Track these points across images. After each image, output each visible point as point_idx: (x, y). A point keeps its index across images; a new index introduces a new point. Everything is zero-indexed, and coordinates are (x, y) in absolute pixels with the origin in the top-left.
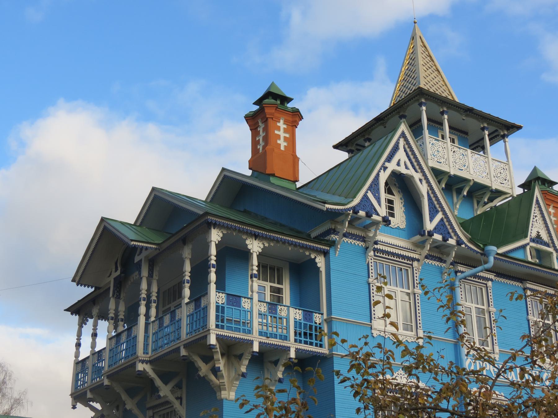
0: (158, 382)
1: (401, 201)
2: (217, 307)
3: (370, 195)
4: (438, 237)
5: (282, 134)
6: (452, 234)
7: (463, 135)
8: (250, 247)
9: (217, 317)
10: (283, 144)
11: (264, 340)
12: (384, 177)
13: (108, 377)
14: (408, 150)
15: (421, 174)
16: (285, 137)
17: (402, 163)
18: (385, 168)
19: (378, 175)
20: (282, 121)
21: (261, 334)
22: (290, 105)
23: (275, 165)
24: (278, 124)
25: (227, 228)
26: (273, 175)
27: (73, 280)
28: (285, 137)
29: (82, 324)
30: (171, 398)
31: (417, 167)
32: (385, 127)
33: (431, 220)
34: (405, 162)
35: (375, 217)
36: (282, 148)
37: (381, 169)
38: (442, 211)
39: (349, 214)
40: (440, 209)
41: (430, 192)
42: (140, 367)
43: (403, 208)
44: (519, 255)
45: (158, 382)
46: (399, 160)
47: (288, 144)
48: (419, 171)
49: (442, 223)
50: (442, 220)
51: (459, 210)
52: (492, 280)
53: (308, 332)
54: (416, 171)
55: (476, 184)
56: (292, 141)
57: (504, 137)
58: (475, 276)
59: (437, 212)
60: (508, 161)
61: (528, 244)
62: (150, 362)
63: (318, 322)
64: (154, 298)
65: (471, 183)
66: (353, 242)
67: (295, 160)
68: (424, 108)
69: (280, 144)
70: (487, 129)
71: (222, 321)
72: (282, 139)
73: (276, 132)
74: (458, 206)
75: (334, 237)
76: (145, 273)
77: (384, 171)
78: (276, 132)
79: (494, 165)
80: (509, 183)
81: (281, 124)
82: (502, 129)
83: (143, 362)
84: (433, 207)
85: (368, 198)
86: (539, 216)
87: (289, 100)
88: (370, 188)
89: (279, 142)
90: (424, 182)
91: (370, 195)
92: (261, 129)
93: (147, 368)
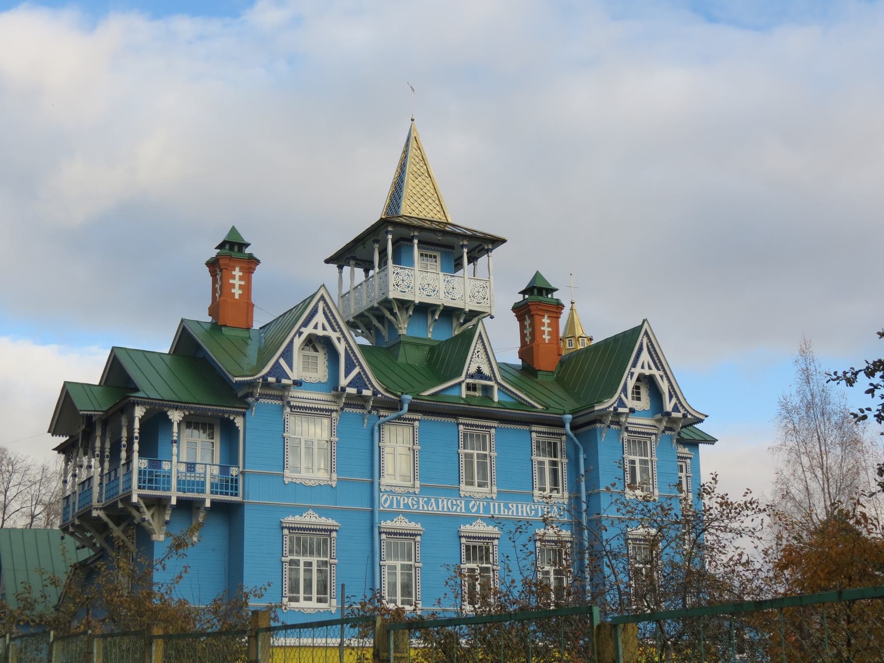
0: (111, 525)
2: (140, 472)
3: (282, 362)
4: (353, 391)
7: (451, 250)
8: (170, 417)
9: (139, 480)
10: (237, 292)
11: (181, 494)
12: (298, 342)
13: (78, 518)
16: (240, 285)
17: (320, 326)
18: (300, 334)
19: (292, 342)
20: (237, 269)
21: (179, 490)
22: (248, 251)
23: (229, 316)
24: (234, 273)
25: (148, 404)
26: (225, 326)
27: (49, 432)
28: (240, 285)
29: (340, 267)
30: (123, 537)
31: (336, 327)
33: (346, 377)
35: (284, 381)
36: (237, 297)
42: (95, 513)
44: (454, 393)
45: (111, 525)
50: (359, 373)
52: (418, 420)
53: (229, 484)
54: (334, 330)
55: (445, 307)
56: (247, 289)
57: (488, 251)
58: (399, 418)
59: (355, 366)
61: (463, 381)
62: (103, 509)
63: (234, 474)
64: (107, 453)
65: (441, 308)
66: (270, 401)
67: (250, 307)
68: (390, 237)
71: (144, 482)
73: (231, 281)
75: (250, 400)
76: (98, 433)
78: (231, 281)
81: (237, 273)
82: (482, 244)
83: (97, 509)
86: (482, 351)
87: (247, 245)
88: (281, 356)
89: (233, 291)
90: (342, 340)
91: (282, 362)
92: (218, 277)
93: (101, 514)
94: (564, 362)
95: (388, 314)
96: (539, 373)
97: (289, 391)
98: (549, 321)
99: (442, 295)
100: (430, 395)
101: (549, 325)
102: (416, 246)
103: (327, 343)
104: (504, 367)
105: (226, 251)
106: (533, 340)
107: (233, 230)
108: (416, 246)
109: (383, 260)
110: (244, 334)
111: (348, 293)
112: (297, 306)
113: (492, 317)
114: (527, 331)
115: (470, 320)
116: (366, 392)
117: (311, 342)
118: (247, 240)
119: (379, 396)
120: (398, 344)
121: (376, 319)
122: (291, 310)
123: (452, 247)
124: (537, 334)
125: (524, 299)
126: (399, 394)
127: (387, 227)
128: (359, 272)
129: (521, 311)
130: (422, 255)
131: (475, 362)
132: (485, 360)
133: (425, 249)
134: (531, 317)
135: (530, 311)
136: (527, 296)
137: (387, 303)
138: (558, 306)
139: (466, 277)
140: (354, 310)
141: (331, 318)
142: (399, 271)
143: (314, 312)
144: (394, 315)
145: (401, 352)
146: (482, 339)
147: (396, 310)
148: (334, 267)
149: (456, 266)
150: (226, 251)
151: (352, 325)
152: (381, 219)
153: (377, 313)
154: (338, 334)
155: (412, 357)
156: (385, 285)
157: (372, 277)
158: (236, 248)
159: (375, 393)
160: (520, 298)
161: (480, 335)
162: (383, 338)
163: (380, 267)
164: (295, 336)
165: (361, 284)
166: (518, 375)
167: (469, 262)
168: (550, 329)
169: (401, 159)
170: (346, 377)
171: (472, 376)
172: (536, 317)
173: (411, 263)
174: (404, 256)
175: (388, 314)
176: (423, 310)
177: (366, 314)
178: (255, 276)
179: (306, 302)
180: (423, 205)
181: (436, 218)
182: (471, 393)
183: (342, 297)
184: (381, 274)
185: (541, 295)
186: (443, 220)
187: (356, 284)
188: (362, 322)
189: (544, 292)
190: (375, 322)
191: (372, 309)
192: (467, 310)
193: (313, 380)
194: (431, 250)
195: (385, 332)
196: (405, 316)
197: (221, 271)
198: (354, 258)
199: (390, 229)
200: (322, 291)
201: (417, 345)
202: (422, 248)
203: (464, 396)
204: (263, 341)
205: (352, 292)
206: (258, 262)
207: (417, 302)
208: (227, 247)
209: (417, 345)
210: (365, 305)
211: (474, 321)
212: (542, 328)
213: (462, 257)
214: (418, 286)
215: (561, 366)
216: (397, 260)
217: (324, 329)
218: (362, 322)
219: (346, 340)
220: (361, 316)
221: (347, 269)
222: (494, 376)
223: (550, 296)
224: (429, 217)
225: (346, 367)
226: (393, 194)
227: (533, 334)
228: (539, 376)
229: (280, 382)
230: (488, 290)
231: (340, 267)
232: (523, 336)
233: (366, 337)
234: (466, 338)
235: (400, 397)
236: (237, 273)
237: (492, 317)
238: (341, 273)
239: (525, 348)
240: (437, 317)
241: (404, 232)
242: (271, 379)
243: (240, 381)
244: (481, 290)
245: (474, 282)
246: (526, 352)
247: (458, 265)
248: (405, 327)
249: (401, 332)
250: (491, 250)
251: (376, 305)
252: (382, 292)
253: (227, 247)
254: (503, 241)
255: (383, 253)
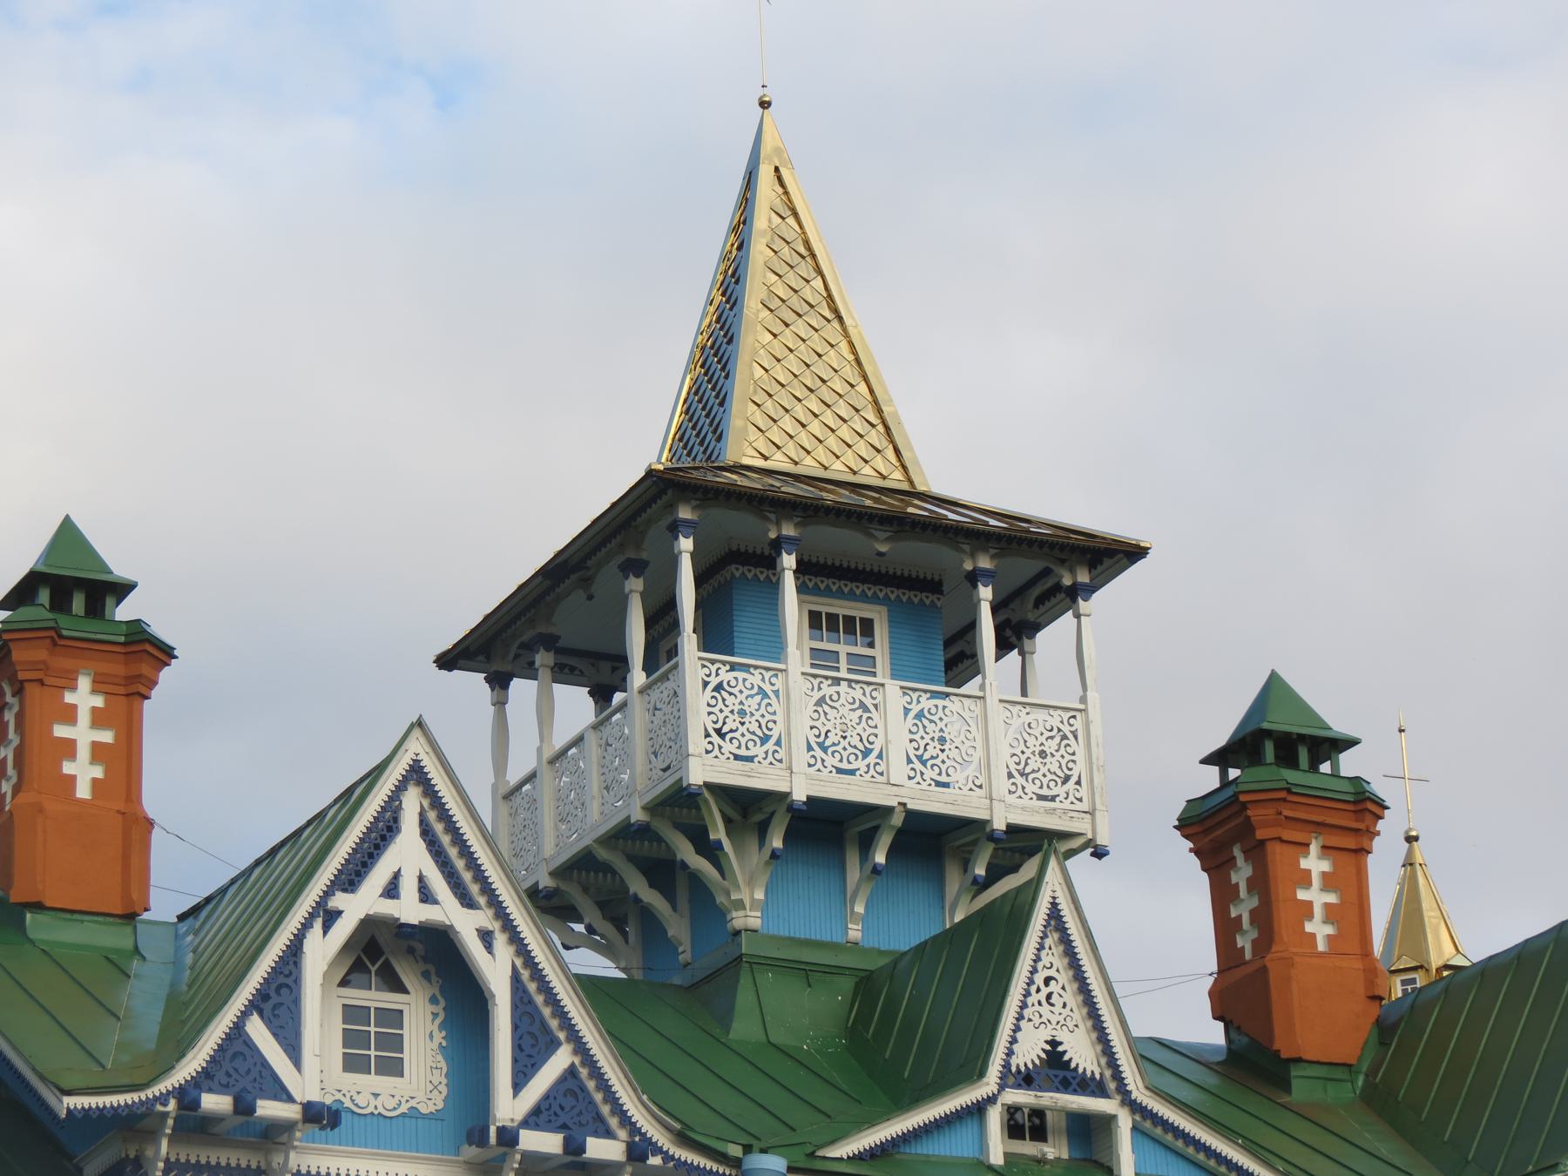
1: (432, 1008)
3: (256, 1029)
4: (547, 1143)
5: (83, 734)
6: (613, 1122)
10: (84, 773)
12: (321, 950)
14: (439, 828)
15: (490, 912)
17: (409, 887)
18: (331, 917)
19: (295, 950)
20: (84, 683)
22: (125, 611)
24: (69, 698)
26: (38, 907)
28: (96, 747)
31: (474, 889)
32: (590, 597)
33: (519, 1082)
34: (421, 879)
35: (268, 1109)
36: (83, 791)
37: (312, 916)
38: (568, 1040)
39: (165, 1115)
40: (562, 1036)
41: (525, 974)
43: (439, 1037)
46: (397, 875)
47: (106, 772)
48: (482, 901)
49: (571, 1084)
50: (571, 1072)
51: (864, 919)
54: (467, 902)
55: (913, 816)
56: (123, 761)
57: (1074, 594)
59: (554, 1045)
60: (1083, 700)
61: (991, 1100)
65: (897, 820)
68: (686, 544)
69: (73, 778)
70: (988, 576)
72: (83, 752)
73: (60, 731)
74: (860, 909)
77: (326, 928)
78: (60, 731)
79: (1016, 723)
80: (1084, 792)
81: (84, 697)
82: (1053, 569)
84: (535, 1029)
85: (249, 1044)
86: (1064, 977)
87: (122, 589)
88: (258, 1004)
89: (68, 768)
90: (500, 940)
91: (256, 1029)
94: (1391, 1028)
95: (686, 852)
96: (1295, 1071)
97: (287, 1147)
98: (1325, 866)
99: (898, 770)
100: (858, 1158)
101: (1328, 882)
102: (789, 582)
103: (438, 953)
104: (1158, 1055)
105: (39, 610)
106: (1265, 941)
107: (68, 534)
108: (789, 582)
109: (665, 646)
110: (114, 938)
111: (531, 777)
112: (320, 816)
113: (1099, 853)
114: (1242, 910)
115: (1015, 869)
116: (600, 1149)
117: (376, 952)
118: (120, 569)
119: (655, 1161)
120: (725, 970)
121: (643, 874)
122: (297, 833)
123: (933, 586)
124: (1283, 916)
125: (1225, 783)
126: (735, 1151)
127: (671, 507)
128: (574, 705)
129: (1216, 830)
130: (815, 620)
131: (1038, 1018)
132: (1079, 1015)
133: (828, 593)
134: (1257, 851)
135: (1248, 828)
136: (1234, 773)
137: (680, 803)
138: (1364, 807)
139: (992, 701)
140: (555, 843)
141: (453, 852)
142: (726, 676)
143: (384, 831)
144: (710, 851)
145: (744, 997)
146: (1062, 929)
147: (718, 833)
148: (472, 684)
149: (950, 665)
150: (39, 610)
151: (551, 905)
152: (650, 473)
153: (645, 848)
154: (484, 917)
155: (792, 1016)
156: (669, 739)
157: (623, 706)
158: (78, 603)
159: (639, 1150)
160: (1209, 779)
161: (1055, 914)
162: (671, 947)
163: (649, 667)
164: (306, 925)
165: (578, 741)
166: (1211, 1080)
167: (1004, 646)
168: (1332, 898)
169: (725, 257)
170: (519, 1082)
171: (1026, 1080)
172: (1276, 852)
173: (775, 648)
174: (745, 624)
175: (686, 852)
176: (826, 830)
177: (603, 854)
178: (153, 710)
179: (350, 799)
180: (815, 427)
181: (867, 475)
182: (1028, 1148)
183: (508, 796)
184: (655, 694)
185: (1293, 763)
186: (896, 479)
187: (560, 739)
188: (579, 891)
189: (1303, 755)
190: (638, 886)
191: (624, 834)
192: (999, 825)
193: (385, 1105)
194: (851, 596)
195: (677, 927)
196: (756, 857)
197: (19, 691)
198: (549, 642)
199: (685, 513)
200: (417, 747)
201: (806, 972)
202: (816, 591)
203: (996, 1157)
204: (189, 959)
205: (546, 775)
206: (164, 654)
207: (799, 795)
208: (44, 596)
209: (806, 972)
210: (599, 815)
211: (1028, 871)
212: (1302, 895)
213: (972, 626)
214: (802, 731)
215: (1384, 1042)
216: (717, 634)
217: (426, 895)
218: (579, 891)
219: (515, 939)
220: (582, 866)
221: (522, 690)
222: (1118, 1076)
223: (1325, 768)
224: (837, 470)
225: (518, 1047)
226: (696, 390)
227: (1264, 917)
228: (1295, 1084)
229: (251, 1110)
230: (1083, 741)
231: (499, 682)
232: (1225, 929)
233: (606, 950)
234: (1000, 931)
235: (736, 1163)
236: (84, 697)
237: (1099, 853)
238: (500, 704)
239: (1239, 973)
240: (880, 858)
241: (742, 527)
242: (214, 1102)
243: (86, 1112)
244: (1051, 746)
245: (1021, 717)
246: (1241, 990)
247: (959, 663)
248: (755, 899)
249: (739, 920)
250: (1090, 590)
251: (638, 815)
252: (660, 763)
253: (44, 596)
254: (1133, 553)
255: (662, 618)
